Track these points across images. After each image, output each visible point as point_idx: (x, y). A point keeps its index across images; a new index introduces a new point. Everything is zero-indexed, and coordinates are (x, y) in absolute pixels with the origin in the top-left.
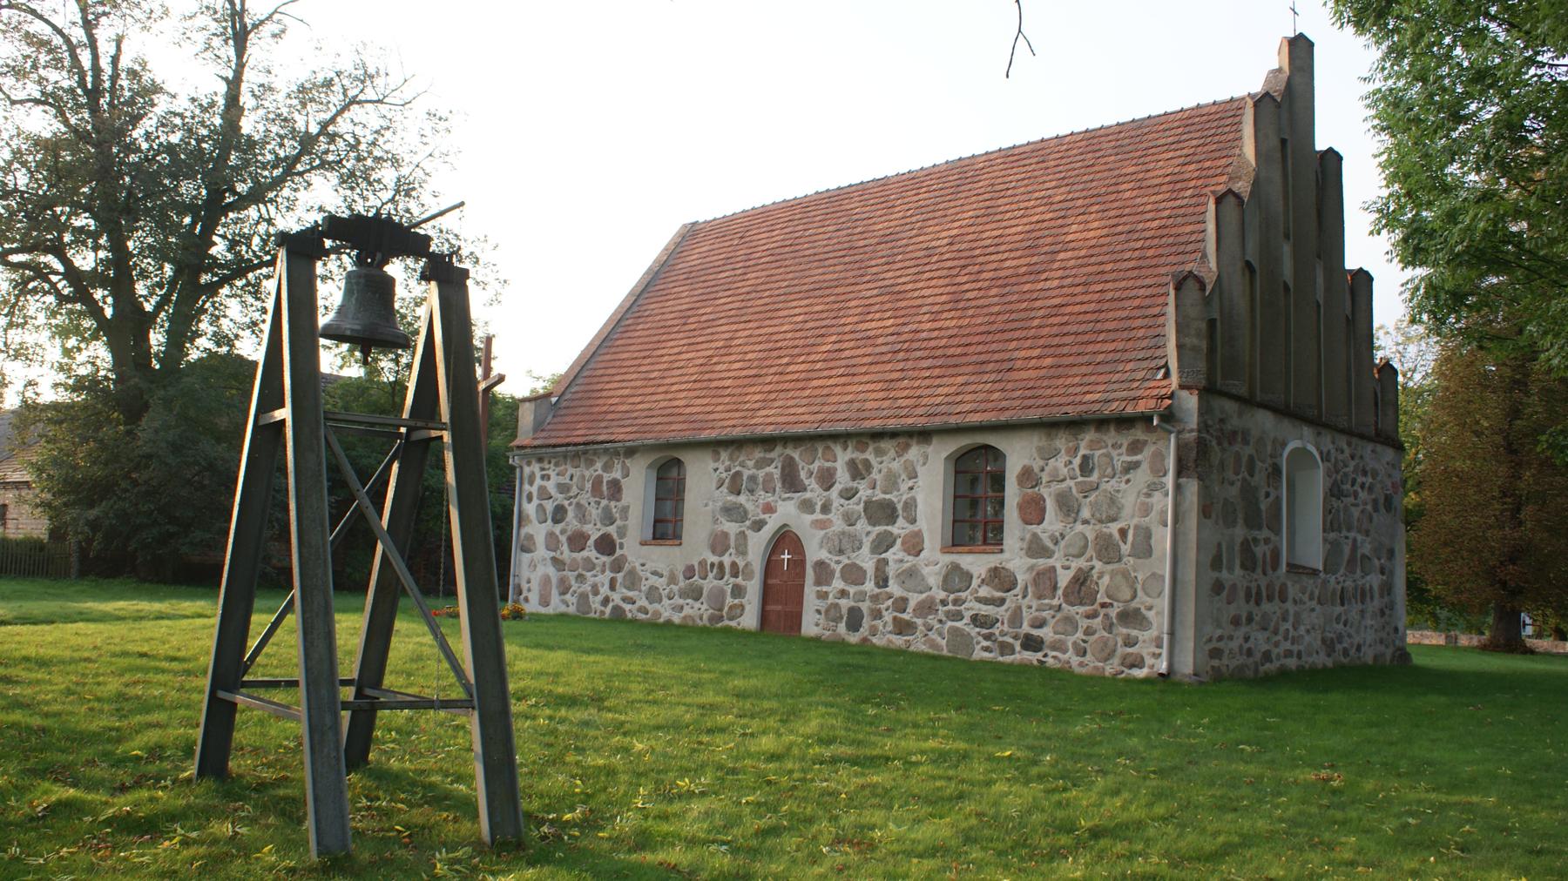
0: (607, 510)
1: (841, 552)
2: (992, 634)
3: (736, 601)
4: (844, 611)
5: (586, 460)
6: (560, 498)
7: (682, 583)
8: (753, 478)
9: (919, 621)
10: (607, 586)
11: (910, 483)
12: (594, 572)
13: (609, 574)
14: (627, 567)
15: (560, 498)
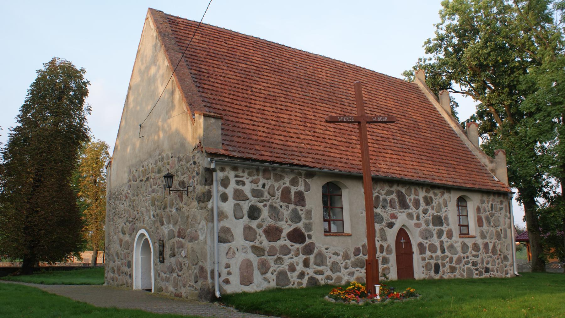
0: (295, 211)
1: (426, 238)
3: (385, 266)
4: (433, 265)
5: (275, 175)
6: (254, 201)
7: (353, 258)
8: (385, 200)
9: (458, 266)
11: (445, 209)
12: (290, 255)
13: (302, 257)
14: (316, 251)
15: (254, 201)
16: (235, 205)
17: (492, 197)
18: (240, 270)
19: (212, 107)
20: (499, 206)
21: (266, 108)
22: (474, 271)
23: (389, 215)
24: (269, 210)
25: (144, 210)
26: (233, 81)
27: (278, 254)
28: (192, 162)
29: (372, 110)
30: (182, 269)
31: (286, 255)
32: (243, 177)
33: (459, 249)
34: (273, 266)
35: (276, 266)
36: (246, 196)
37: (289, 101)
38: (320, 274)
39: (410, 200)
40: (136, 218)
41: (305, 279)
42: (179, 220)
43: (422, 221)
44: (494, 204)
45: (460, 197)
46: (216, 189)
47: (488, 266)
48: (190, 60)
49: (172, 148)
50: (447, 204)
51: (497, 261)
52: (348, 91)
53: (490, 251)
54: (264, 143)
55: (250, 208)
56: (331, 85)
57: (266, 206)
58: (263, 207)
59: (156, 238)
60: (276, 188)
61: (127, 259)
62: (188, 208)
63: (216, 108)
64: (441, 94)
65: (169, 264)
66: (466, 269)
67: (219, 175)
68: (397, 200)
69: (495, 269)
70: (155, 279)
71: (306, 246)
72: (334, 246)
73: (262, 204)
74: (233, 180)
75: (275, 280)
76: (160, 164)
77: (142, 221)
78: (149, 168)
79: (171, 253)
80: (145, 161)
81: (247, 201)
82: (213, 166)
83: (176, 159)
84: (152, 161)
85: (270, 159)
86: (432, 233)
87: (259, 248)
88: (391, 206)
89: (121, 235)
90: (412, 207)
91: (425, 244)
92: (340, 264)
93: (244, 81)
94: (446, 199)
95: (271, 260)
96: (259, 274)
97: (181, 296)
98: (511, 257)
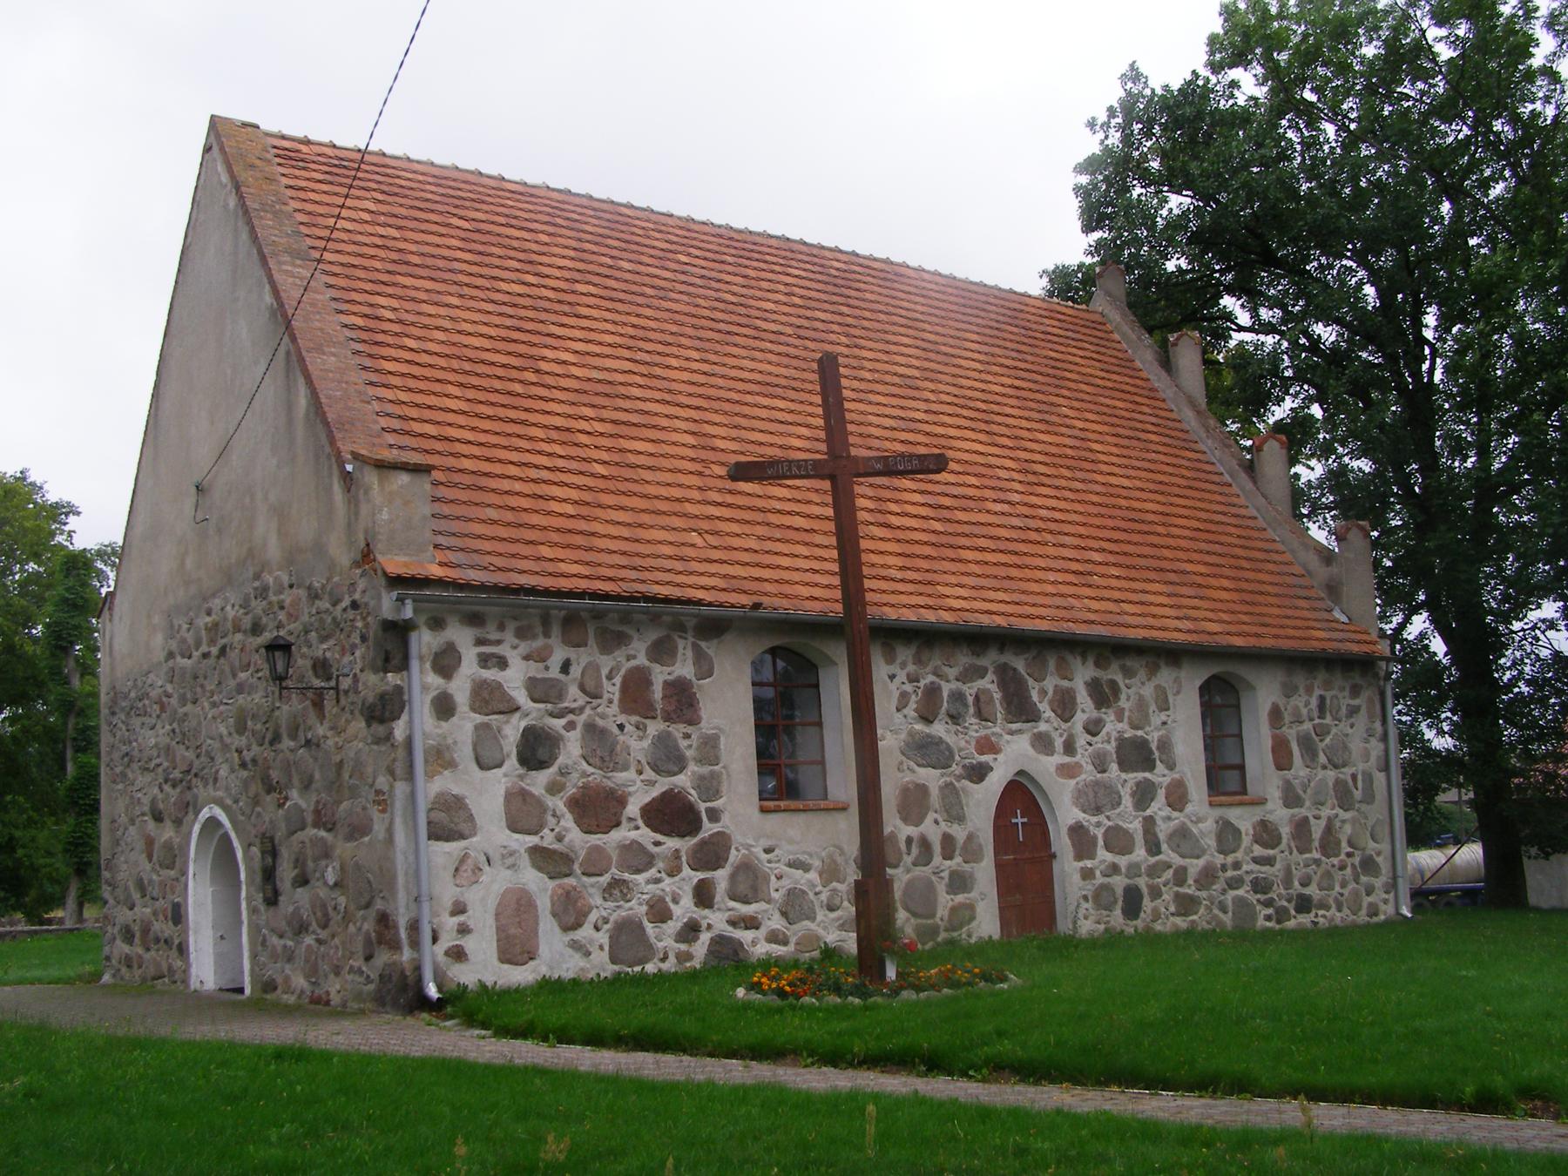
0: (663, 740)
1: (1098, 810)
2: (1272, 900)
3: (960, 898)
4: (1119, 892)
6: (533, 712)
8: (958, 697)
9: (1203, 894)
10: (687, 901)
11: (1163, 717)
12: (652, 873)
14: (734, 856)
16: (477, 728)
17: (1322, 675)
18: (497, 919)
19: (407, 433)
20: (1346, 701)
21: (583, 425)
22: (1258, 908)
23: (973, 743)
24: (583, 738)
25: (217, 745)
26: (476, 342)
27: (614, 870)
28: (346, 602)
29: (934, 407)
30: (329, 920)
31: (638, 871)
32: (499, 642)
33: (1211, 842)
34: (600, 908)
35: (611, 904)
36: (511, 699)
37: (658, 395)
38: (747, 928)
39: (1043, 692)
40: (194, 771)
41: (700, 942)
42: (317, 776)
43: (1082, 758)
44: (1328, 695)
45: (1214, 678)
46: (423, 682)
47: (1306, 891)
48: (342, 282)
49: (290, 560)
50: (1166, 700)
51: (1338, 876)
52: (857, 352)
53: (1316, 844)
54: (568, 535)
55: (523, 734)
56: (802, 332)
57: (574, 728)
58: (563, 732)
59: (254, 832)
60: (604, 672)
61: (170, 897)
62: (340, 741)
63: (421, 435)
64: (1175, 344)
65: (291, 909)
66: (1230, 903)
67: (424, 641)
68: (997, 696)
69: (1331, 901)
70: (254, 956)
71: (703, 843)
72: (791, 841)
73: (563, 722)
74: (469, 655)
75: (607, 948)
76: (258, 606)
77: (211, 781)
78: (225, 619)
79: (297, 876)
80: (214, 595)
81: (517, 715)
82: (408, 612)
83: (302, 593)
84: (233, 597)
85: (583, 584)
86: (1118, 793)
87: (554, 852)
88: (980, 715)
89: (151, 824)
90: (1049, 714)
91: (1091, 828)
92: (811, 895)
93: (515, 341)
94: (1165, 685)
95: (592, 889)
96: (557, 929)
97: (327, 1003)
98: (1389, 864)
